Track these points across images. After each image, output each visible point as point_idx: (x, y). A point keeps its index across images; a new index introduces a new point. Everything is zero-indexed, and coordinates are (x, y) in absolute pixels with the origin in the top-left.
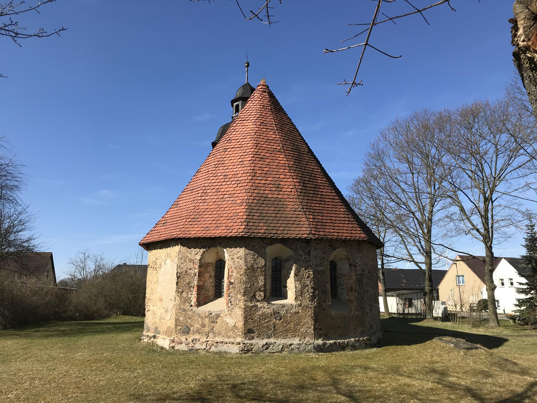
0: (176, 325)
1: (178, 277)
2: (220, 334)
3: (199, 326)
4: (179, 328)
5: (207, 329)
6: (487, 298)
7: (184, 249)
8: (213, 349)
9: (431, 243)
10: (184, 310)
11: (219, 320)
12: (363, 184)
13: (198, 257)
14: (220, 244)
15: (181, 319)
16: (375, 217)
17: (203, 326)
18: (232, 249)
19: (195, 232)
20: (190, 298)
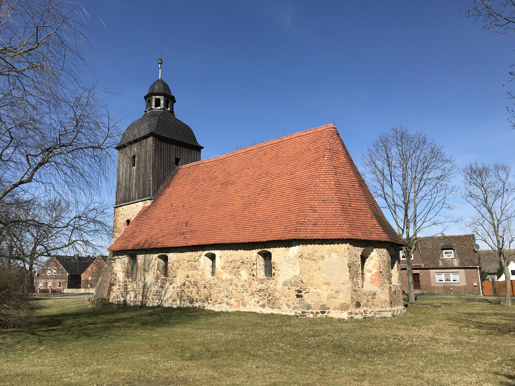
0: (352, 302)
1: (349, 267)
2: (377, 306)
3: (366, 302)
4: (354, 303)
5: (370, 303)
6: (466, 284)
7: (351, 247)
8: (377, 316)
9: (36, 238)
10: (356, 291)
11: (376, 297)
12: (429, 272)
13: (360, 253)
14: (372, 245)
15: (354, 297)
16: (418, 326)
17: (368, 301)
18: (379, 249)
19: (360, 236)
20: (358, 282)
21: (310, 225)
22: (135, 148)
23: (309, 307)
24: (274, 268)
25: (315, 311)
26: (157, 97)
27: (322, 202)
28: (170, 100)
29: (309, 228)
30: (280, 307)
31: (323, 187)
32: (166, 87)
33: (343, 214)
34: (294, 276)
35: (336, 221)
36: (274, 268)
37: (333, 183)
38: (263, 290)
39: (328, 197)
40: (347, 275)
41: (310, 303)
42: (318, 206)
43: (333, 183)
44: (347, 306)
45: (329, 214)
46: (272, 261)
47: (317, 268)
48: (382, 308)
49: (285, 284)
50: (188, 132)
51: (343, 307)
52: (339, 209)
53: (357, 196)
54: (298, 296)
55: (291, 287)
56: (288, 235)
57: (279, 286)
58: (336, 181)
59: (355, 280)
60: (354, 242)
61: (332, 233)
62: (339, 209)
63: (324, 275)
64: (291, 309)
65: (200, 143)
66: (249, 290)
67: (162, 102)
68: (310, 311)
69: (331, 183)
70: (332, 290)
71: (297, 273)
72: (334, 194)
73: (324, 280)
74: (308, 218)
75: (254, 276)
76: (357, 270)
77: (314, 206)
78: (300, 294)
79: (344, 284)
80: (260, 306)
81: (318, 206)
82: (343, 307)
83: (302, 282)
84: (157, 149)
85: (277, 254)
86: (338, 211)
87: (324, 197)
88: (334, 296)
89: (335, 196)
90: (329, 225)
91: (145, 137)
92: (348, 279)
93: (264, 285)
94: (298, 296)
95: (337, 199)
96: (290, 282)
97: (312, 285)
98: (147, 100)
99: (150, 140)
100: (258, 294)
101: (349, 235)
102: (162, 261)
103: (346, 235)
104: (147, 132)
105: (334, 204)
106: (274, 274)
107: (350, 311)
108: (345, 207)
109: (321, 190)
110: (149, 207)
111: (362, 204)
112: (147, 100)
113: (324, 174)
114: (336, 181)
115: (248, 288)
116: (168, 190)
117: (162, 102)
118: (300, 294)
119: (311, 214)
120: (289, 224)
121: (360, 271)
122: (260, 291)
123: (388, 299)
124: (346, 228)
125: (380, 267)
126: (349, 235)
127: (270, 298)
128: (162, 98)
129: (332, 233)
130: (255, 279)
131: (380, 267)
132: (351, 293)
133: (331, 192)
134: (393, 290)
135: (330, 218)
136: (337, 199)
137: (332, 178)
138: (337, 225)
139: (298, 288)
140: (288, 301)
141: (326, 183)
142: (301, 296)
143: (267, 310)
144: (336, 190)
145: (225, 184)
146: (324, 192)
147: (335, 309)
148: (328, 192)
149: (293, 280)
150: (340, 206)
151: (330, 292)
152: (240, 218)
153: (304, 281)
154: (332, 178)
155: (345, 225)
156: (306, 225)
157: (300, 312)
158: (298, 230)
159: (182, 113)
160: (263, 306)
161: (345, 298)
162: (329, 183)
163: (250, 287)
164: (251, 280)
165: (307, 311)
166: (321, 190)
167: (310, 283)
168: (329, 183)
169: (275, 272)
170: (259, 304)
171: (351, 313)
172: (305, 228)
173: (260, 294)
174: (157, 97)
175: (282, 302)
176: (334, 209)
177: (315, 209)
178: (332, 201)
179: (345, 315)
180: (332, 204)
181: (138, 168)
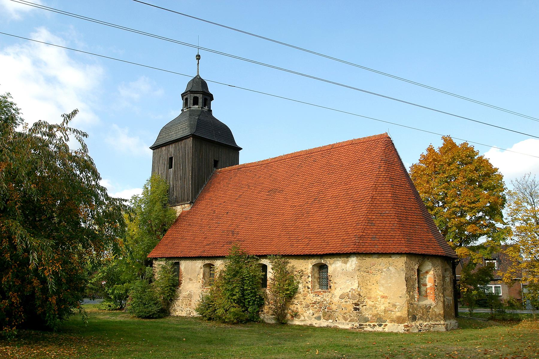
0: (408, 315)
4: (410, 316)
15: (411, 310)
21: (368, 239)
22: (172, 148)
23: (366, 320)
24: (330, 281)
25: (372, 324)
26: (196, 95)
27: (379, 215)
28: (208, 98)
29: (367, 241)
30: (337, 319)
31: (380, 200)
32: (204, 84)
33: (401, 228)
34: (352, 289)
35: (394, 235)
36: (330, 281)
37: (390, 195)
38: (319, 303)
39: (385, 210)
40: (404, 289)
41: (367, 316)
42: (376, 220)
43: (390, 195)
44: (403, 319)
45: (387, 227)
46: (329, 274)
47: (374, 282)
48: (437, 321)
49: (342, 297)
50: (225, 132)
51: (400, 320)
52: (396, 222)
53: (413, 209)
54: (356, 309)
55: (347, 300)
56: (346, 249)
57: (336, 299)
58: (393, 193)
59: (411, 293)
60: (409, 255)
61: (391, 247)
62: (396, 222)
63: (382, 289)
64: (347, 322)
65: (239, 144)
66: (303, 303)
67: (200, 101)
68: (367, 323)
69: (388, 195)
70: (389, 303)
71: (355, 286)
72: (391, 207)
73: (381, 294)
74: (366, 232)
75: (308, 288)
76: (415, 284)
77: (372, 219)
78: (358, 307)
79: (400, 297)
80: (315, 318)
81: (376, 220)
82: (400, 320)
83: (360, 295)
84: (196, 150)
85: (335, 266)
86: (395, 225)
87: (381, 210)
88: (391, 309)
89: (393, 209)
90: (387, 239)
91: (186, 138)
92: (405, 292)
93: (319, 298)
94: (356, 309)
95: (394, 212)
96: (348, 295)
97: (369, 298)
98: (185, 97)
99: (190, 141)
100: (313, 306)
101: (407, 249)
102: (208, 270)
103: (405, 249)
104: (187, 132)
105: (391, 217)
106: (330, 287)
107: (406, 324)
108: (403, 220)
109: (378, 202)
110: (188, 212)
111: (418, 217)
112: (185, 97)
113: (381, 186)
114: (393, 193)
115: (303, 300)
116: (208, 195)
117: (200, 101)
118: (358, 307)
119: (368, 227)
120: (346, 237)
121: (417, 285)
122: (315, 303)
123: (442, 312)
124: (404, 242)
125: (435, 281)
126: (407, 249)
127: (326, 310)
128: (200, 96)
129: (391, 247)
130: (310, 292)
131: (435, 281)
132: (408, 307)
133: (388, 205)
134: (446, 303)
135: (388, 232)
136: (394, 212)
137: (389, 190)
138: (395, 239)
139: (355, 301)
140: (345, 313)
141: (383, 195)
142: (358, 309)
143: (324, 323)
144: (393, 202)
145: (272, 191)
146: (381, 205)
147: (392, 321)
148: (385, 205)
149: (350, 293)
150: (397, 220)
151: (387, 305)
152: (292, 228)
153: (361, 294)
154: (389, 190)
155: (403, 239)
156: (364, 239)
157: (358, 325)
158: (357, 244)
159: (219, 111)
160: (319, 318)
161: (401, 311)
162: (386, 195)
163: (304, 299)
164: (305, 292)
165: (364, 324)
166: (378, 202)
167: (368, 296)
168: (386, 195)
169: (332, 285)
170: (314, 316)
171: (407, 326)
172: (364, 241)
173: (315, 306)
174: (196, 95)
175: (339, 314)
176: (392, 222)
177: (373, 222)
178: (390, 215)
179: (400, 328)
180: (389, 217)
181: (175, 172)
